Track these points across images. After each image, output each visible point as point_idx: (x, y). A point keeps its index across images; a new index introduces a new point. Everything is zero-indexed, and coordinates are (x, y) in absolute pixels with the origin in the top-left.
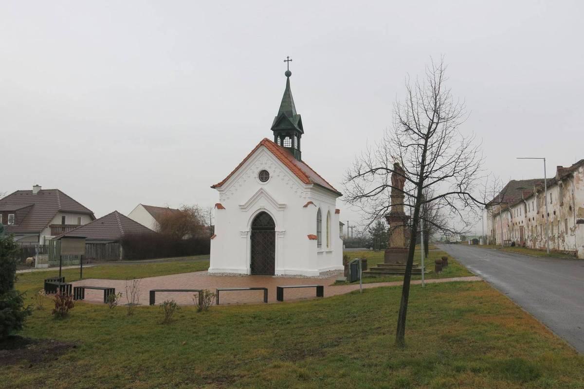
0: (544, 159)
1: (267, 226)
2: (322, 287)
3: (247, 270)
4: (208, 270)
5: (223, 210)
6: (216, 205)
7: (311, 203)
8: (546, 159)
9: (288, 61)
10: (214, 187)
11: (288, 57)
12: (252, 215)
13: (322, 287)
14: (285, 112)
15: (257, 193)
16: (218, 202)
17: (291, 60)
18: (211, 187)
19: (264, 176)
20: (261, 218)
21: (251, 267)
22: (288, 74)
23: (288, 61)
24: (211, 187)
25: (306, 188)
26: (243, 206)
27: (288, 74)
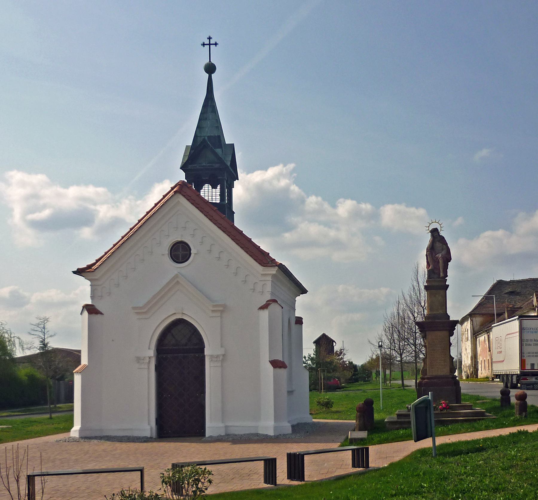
0: (142, 471)
1: (186, 345)
2: (274, 460)
3: (151, 429)
4: (70, 431)
5: (99, 316)
6: (83, 307)
7: (275, 301)
8: (145, 471)
9: (210, 44)
10: (79, 272)
11: (204, 45)
12: (163, 321)
13: (274, 460)
14: (206, 138)
15: (168, 284)
16: (90, 302)
17: (216, 44)
18: (74, 272)
19: (180, 252)
20: (169, 337)
21: (157, 423)
22: (210, 69)
23: (210, 44)
24: (74, 272)
25: (213, 311)
26: (141, 308)
27: (210, 69)
